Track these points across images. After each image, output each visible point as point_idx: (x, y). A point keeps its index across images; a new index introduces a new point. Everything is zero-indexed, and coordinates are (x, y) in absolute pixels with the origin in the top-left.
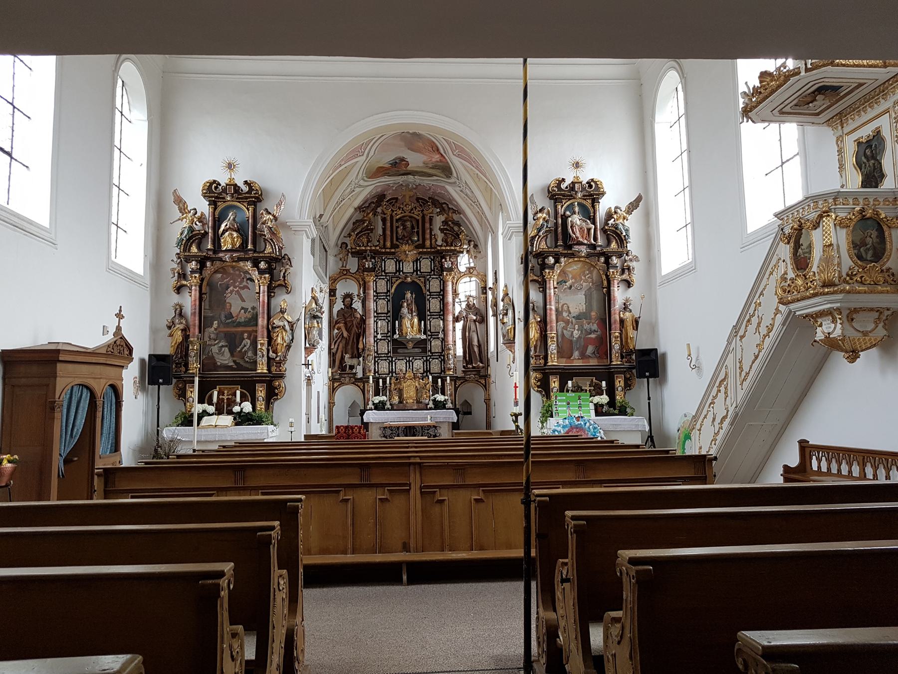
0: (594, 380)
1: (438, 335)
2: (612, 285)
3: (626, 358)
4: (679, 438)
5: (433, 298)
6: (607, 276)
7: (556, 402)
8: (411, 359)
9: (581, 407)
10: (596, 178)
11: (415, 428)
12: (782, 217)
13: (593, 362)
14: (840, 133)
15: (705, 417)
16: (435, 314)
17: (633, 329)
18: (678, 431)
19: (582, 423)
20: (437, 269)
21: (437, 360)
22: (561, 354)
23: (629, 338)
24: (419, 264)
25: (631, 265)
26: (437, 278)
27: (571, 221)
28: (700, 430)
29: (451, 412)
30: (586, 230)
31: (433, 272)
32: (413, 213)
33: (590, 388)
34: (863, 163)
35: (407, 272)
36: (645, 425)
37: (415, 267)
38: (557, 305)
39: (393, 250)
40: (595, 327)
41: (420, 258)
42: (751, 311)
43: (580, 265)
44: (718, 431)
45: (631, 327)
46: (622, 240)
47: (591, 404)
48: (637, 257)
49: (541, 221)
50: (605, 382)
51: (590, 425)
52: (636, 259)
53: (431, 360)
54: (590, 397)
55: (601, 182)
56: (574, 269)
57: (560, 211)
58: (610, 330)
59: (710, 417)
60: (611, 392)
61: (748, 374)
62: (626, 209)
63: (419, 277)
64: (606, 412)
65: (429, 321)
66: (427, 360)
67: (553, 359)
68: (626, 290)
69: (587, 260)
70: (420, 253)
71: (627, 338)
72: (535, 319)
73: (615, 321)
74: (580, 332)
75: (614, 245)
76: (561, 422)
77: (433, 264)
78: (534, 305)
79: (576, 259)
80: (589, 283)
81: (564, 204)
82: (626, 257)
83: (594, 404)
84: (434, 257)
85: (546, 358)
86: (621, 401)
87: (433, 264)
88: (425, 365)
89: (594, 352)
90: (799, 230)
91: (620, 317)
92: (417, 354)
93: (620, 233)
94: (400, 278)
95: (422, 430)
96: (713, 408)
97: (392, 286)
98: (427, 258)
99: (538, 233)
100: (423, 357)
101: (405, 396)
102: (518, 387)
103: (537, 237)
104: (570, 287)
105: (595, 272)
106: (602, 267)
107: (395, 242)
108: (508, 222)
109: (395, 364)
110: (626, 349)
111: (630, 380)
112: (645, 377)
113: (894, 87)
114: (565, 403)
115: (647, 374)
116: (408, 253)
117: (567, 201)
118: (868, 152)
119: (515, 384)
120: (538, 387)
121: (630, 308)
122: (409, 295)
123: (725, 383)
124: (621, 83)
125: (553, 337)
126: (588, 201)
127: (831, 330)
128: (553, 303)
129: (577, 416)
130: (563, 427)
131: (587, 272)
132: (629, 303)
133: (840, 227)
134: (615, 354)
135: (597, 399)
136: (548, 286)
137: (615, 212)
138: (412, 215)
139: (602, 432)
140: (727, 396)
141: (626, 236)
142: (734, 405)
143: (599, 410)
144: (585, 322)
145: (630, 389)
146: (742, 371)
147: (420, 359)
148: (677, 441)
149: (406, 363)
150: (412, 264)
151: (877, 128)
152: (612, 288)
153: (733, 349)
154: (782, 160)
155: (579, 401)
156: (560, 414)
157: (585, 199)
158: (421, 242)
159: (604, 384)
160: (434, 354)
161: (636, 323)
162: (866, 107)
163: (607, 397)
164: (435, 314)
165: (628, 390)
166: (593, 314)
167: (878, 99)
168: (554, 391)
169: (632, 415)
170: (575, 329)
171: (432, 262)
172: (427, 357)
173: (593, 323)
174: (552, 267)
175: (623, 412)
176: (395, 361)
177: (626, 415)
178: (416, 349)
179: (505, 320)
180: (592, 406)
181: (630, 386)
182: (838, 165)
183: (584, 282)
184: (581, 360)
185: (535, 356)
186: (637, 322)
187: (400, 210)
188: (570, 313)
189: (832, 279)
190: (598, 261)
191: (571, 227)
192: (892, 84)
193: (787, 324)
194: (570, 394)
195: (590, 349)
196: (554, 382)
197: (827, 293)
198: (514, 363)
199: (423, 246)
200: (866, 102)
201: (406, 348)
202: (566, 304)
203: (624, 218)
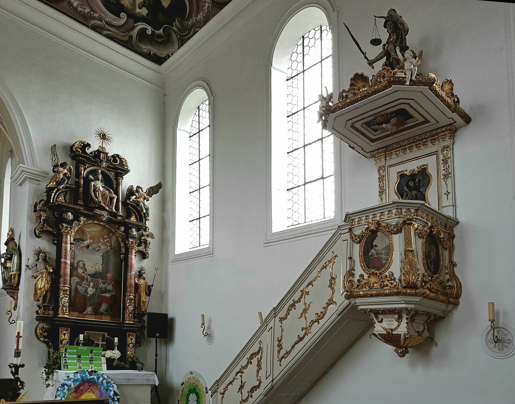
0: (106, 336)
4: (182, 391)
6: (126, 245)
7: (65, 354)
9: (92, 360)
10: (122, 155)
12: (353, 218)
13: (106, 319)
14: (382, 163)
15: (231, 383)
17: (146, 295)
18: (182, 385)
19: (95, 377)
22: (72, 307)
23: (142, 302)
25: (148, 239)
27: (94, 185)
28: (223, 394)
30: (108, 197)
33: (102, 343)
34: (405, 192)
38: (72, 261)
40: (110, 287)
42: (296, 297)
43: (99, 228)
44: (247, 398)
46: (142, 216)
47: (102, 357)
48: (152, 235)
49: (61, 176)
50: (117, 338)
51: (103, 380)
52: (152, 236)
55: (126, 161)
57: (83, 173)
58: (125, 292)
59: (237, 384)
60: (122, 347)
61: (288, 353)
62: (147, 191)
72: (46, 269)
73: (131, 285)
74: (94, 290)
75: (133, 219)
76: (72, 376)
78: (46, 255)
79: (95, 222)
80: (107, 247)
81: (88, 168)
82: (144, 232)
83: (106, 358)
85: (56, 310)
86: (132, 356)
89: (107, 311)
90: (373, 234)
91: (135, 282)
93: (140, 210)
96: (241, 376)
99: (58, 186)
102: (21, 337)
103: (56, 190)
104: (88, 247)
105: (114, 239)
106: (121, 234)
108: (21, 165)
113: (446, 134)
114: (75, 356)
115: (158, 335)
117: (91, 166)
118: (411, 184)
119: (19, 333)
120: (45, 337)
121: (144, 276)
123: (259, 356)
124: (148, 85)
127: (393, 327)
128: (69, 257)
129: (90, 370)
130: (74, 381)
131: (106, 236)
132: (143, 272)
133: (419, 237)
134: (129, 313)
135: (109, 354)
136: (64, 240)
137: (137, 191)
139: (115, 386)
140: (260, 369)
142: (270, 379)
143: (111, 364)
144: (100, 281)
146: (281, 349)
148: (181, 393)
151: (423, 166)
152: (129, 256)
153: (271, 328)
154: (305, 181)
155: (90, 355)
157: (109, 171)
159: (116, 340)
161: (149, 290)
162: (413, 146)
163: (118, 352)
165: (138, 346)
166: (109, 275)
167: (426, 142)
168: (63, 343)
169: (142, 369)
170: (89, 286)
174: (70, 223)
175: (133, 366)
177: (137, 370)
179: (8, 265)
180: (103, 360)
182: (377, 190)
184: (94, 316)
185: (44, 306)
188: (85, 270)
189: (416, 282)
190: (119, 229)
192: (444, 131)
193: (341, 315)
194: (81, 347)
195: (104, 307)
196: (64, 334)
197: (409, 295)
198: (15, 310)
200: (414, 142)
202: (82, 261)
203: (144, 199)
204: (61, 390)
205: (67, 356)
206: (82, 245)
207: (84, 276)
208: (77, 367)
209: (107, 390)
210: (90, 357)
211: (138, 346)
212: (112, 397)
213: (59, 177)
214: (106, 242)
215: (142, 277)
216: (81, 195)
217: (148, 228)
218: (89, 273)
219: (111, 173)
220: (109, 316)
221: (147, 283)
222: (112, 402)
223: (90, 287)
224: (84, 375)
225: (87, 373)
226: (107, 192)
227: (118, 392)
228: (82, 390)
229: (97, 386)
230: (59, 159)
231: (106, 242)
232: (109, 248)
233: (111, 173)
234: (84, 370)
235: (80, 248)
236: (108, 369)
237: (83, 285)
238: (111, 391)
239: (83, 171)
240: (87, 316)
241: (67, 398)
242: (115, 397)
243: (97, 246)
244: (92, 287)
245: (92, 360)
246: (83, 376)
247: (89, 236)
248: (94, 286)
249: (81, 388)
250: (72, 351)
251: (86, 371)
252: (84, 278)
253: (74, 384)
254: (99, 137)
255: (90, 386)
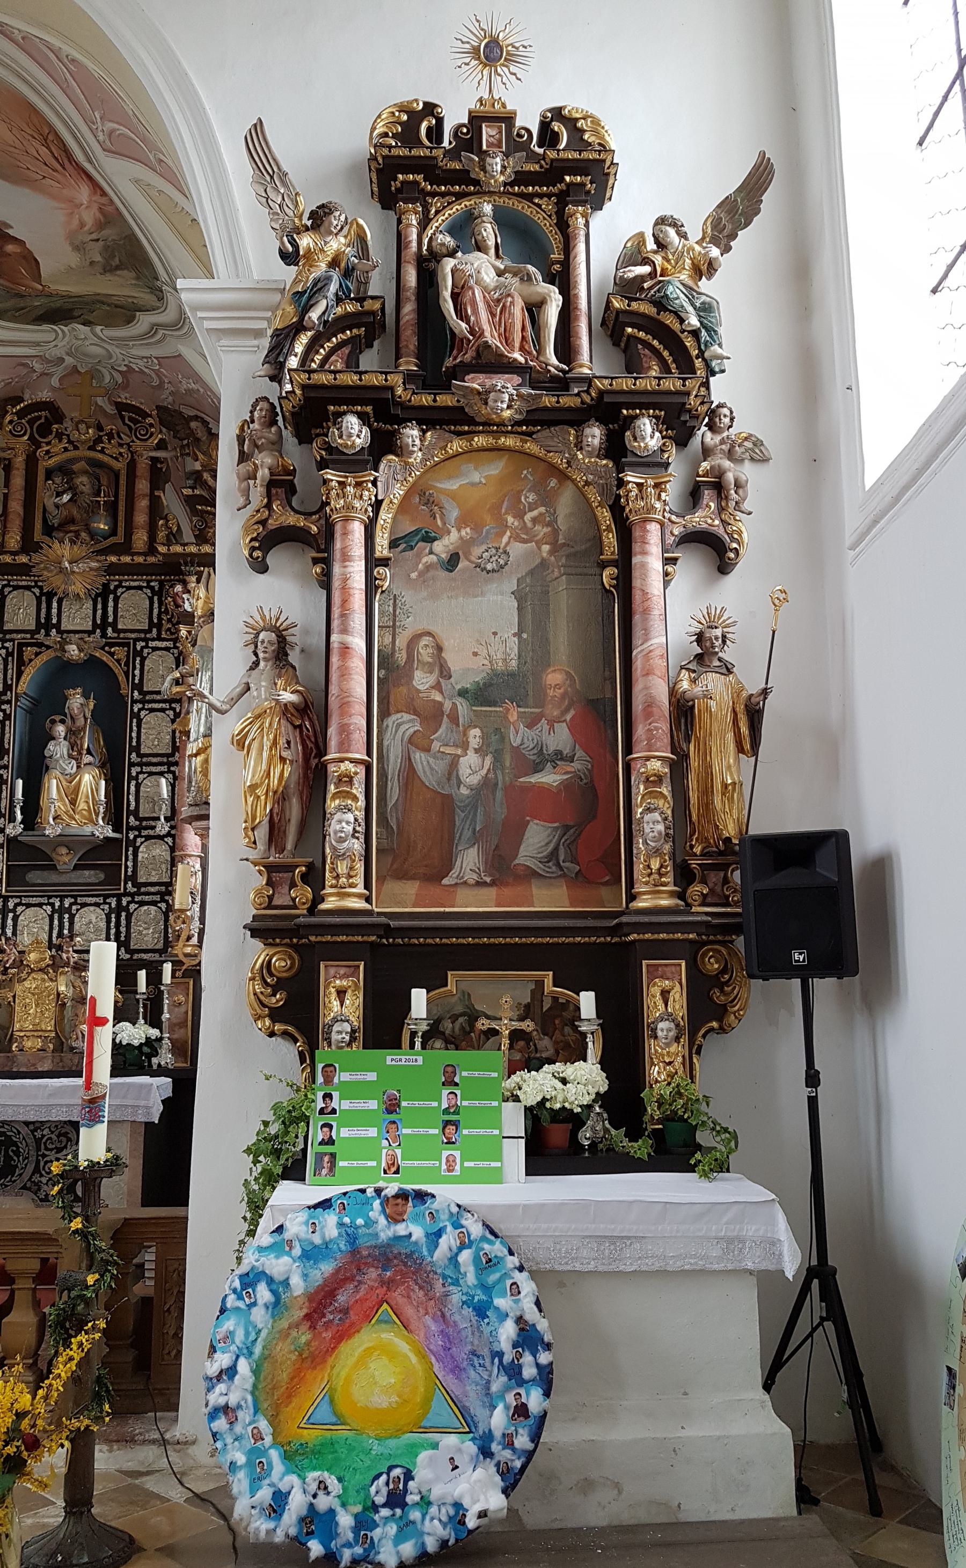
1: (153, 828)
2: (636, 547)
3: (704, 881)
5: (152, 710)
6: (617, 509)
7: (328, 1096)
8: (67, 903)
9: (456, 1124)
10: (574, 103)
11: (15, 1144)
16: (154, 760)
17: (740, 749)
20: (169, 621)
21: (153, 908)
23: (718, 786)
24: (111, 604)
26: (167, 649)
27: (453, 272)
29: (141, 1086)
31: (155, 630)
32: (102, 451)
35: (72, 628)
36: (774, 1242)
37: (99, 612)
39: (24, 559)
41: (116, 587)
43: (495, 468)
45: (730, 736)
48: (758, 443)
50: (592, 994)
51: (462, 1246)
53: (132, 907)
54: (511, 1072)
56: (473, 484)
58: (628, 750)
62: (704, 232)
63: (112, 645)
64: (593, 1145)
65: (133, 783)
66: (119, 909)
67: (343, 880)
68: (711, 582)
69: (530, 446)
70: (112, 570)
71: (707, 791)
73: (650, 705)
74: (488, 760)
77: (156, 605)
80: (539, 544)
82: (709, 435)
84: (161, 583)
87: (156, 605)
88: (113, 924)
89: (554, 855)
91: (672, 692)
92: (88, 889)
94: (48, 647)
95: (38, 1149)
97: (20, 674)
98: (140, 588)
100: (106, 897)
101: (17, 1026)
104: (452, 561)
105: (565, 502)
107: (38, 536)
109: (15, 919)
110: (703, 840)
111: (721, 986)
112: (787, 970)
114: (373, 1105)
115: (799, 957)
116: (67, 564)
122: (76, 701)
125: (348, 779)
126: (543, 202)
129: (391, 1189)
132: (718, 632)
134: (648, 857)
137: (661, 245)
138: (100, 456)
139: (528, 1287)
141: (704, 333)
144: (513, 716)
145: (722, 1030)
147: (97, 905)
149: (51, 918)
150: (89, 604)
155: (445, 1092)
156: (341, 1164)
157: (529, 197)
158: (120, 538)
159: (587, 1002)
160: (143, 890)
164: (154, 760)
166: (554, 678)
168: (335, 1037)
170: (465, 746)
171: (156, 598)
172: (119, 897)
173: (551, 724)
176: (14, 911)
178: (87, 873)
181: (721, 1012)
183: (516, 538)
184: (492, 892)
186: (754, 715)
187: (60, 441)
188: (445, 672)
190: (579, 446)
191: (455, 297)
196: (341, 993)
199: (126, 548)
201: (53, 868)
202: (429, 634)
204: (238, 1308)
205: (335, 1104)
206: (424, 560)
207: (441, 704)
208: (379, 1163)
209: (481, 1311)
210: (445, 1105)
211: (712, 1029)
212: (507, 1358)
213: (308, 277)
214: (529, 525)
215: (717, 663)
216: (410, 332)
217: (725, 411)
218: (458, 687)
219: (539, 206)
220: (563, 880)
221: (743, 689)
222: (507, 1389)
223: (470, 753)
224: (360, 1221)
225: (377, 1204)
226: (512, 282)
227: (542, 1325)
228: (345, 1311)
229: (426, 1287)
230: (297, 194)
231: (529, 525)
232: (546, 548)
233: (539, 206)
234: (363, 1191)
235: (420, 575)
236: (533, 1169)
237: (436, 746)
238: (504, 1316)
239: (415, 230)
240: (462, 893)
241: (264, 1358)
242: (527, 1358)
243: (494, 551)
244: (476, 751)
245: (456, 1124)
246: (357, 1228)
247: (454, 514)
248: (488, 746)
249: (342, 1298)
250: (359, 1077)
251: (370, 1192)
252: (443, 713)
253: (305, 1276)
254: (474, 63)
255: (389, 1284)
